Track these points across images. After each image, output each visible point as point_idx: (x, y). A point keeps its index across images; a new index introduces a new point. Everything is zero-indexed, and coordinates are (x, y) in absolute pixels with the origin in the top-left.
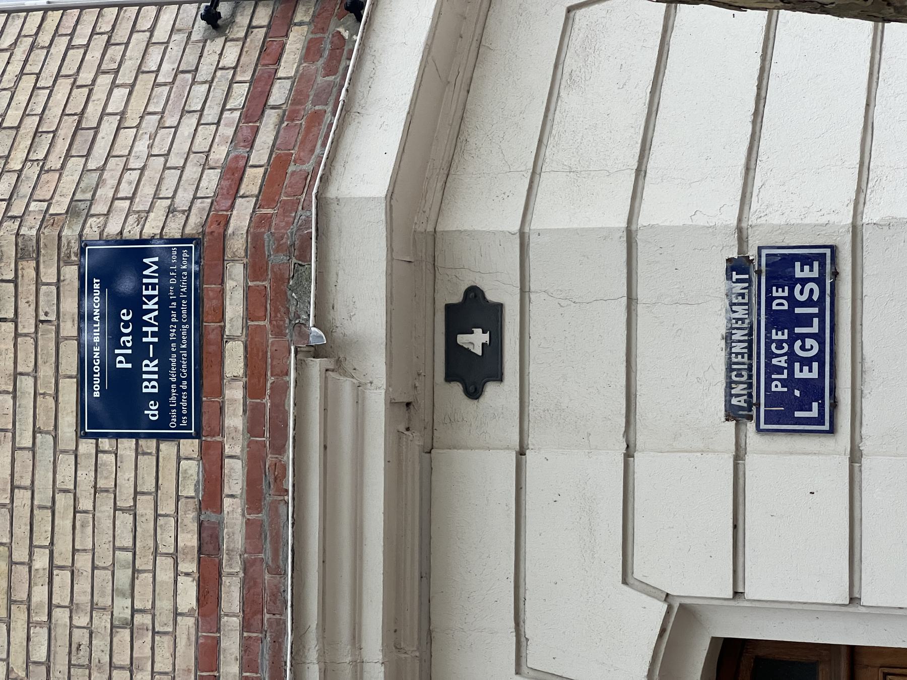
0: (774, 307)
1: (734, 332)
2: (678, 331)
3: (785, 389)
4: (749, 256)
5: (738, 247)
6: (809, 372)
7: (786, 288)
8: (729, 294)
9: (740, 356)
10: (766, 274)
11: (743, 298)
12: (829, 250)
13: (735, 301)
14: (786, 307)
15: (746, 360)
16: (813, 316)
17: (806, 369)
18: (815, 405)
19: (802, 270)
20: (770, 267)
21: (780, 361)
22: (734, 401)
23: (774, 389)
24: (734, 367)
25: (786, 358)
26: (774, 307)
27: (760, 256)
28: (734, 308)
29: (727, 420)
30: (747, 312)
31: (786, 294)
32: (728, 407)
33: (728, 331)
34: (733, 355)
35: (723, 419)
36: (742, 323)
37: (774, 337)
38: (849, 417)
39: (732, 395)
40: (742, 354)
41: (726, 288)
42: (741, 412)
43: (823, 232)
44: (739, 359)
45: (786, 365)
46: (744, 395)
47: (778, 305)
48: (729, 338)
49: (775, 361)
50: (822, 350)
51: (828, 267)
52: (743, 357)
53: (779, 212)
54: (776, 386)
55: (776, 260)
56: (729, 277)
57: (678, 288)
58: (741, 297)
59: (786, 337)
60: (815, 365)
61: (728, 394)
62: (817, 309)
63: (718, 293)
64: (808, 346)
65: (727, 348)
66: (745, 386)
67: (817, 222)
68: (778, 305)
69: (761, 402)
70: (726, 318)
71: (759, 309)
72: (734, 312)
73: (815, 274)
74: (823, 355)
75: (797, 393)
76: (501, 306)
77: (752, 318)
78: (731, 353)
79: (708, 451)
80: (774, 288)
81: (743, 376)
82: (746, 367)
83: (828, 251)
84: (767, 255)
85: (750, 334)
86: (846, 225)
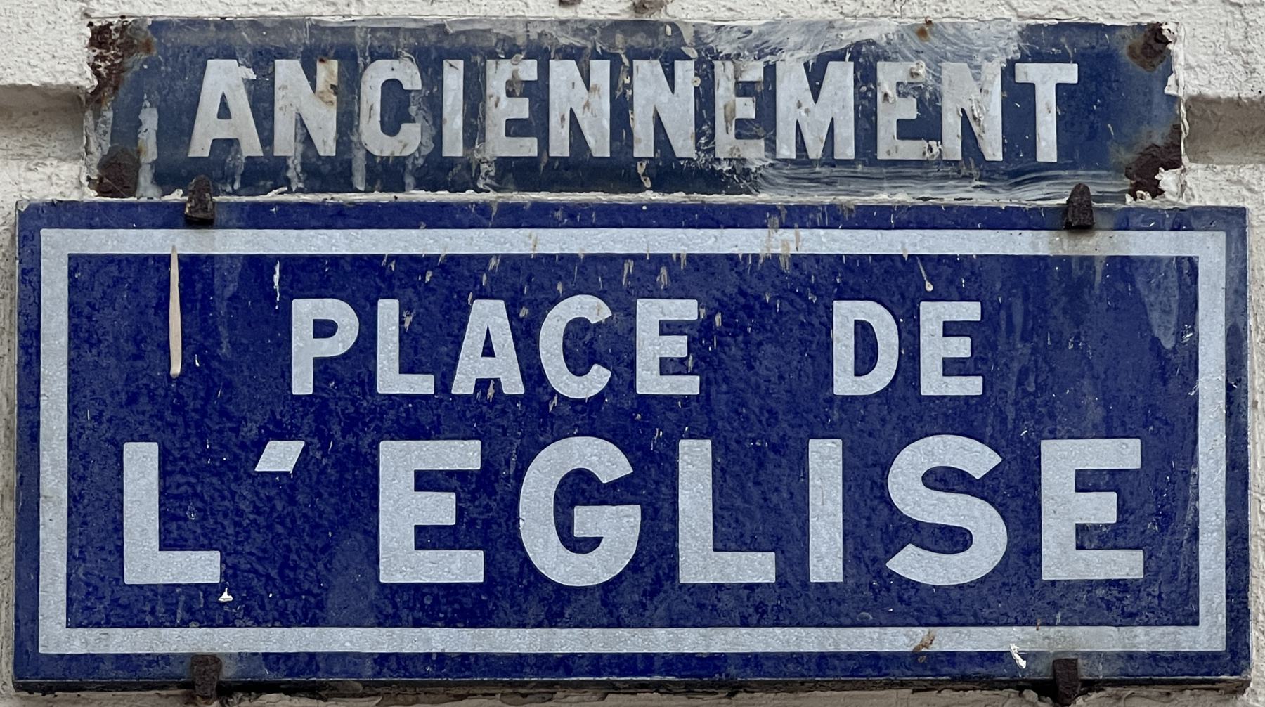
0: (846, 313)
1: (685, 71)
3: (303, 384)
4: (1174, 164)
6: (419, 530)
7: (972, 386)
8: (935, 41)
9: (521, 108)
10: (1065, 261)
11: (906, 130)
12: (1219, 645)
13: (889, 76)
14: (846, 383)
15: (499, 145)
19: (1086, 482)
20: (1107, 285)
21: (488, 351)
23: (305, 311)
24: (454, 77)
25: (514, 385)
26: (846, 313)
27: (1183, 220)
28: (841, 76)
29: (100, 37)
30: (815, 151)
31: (933, 383)
32: (189, 38)
33: (688, 36)
34: (529, 70)
36: (741, 123)
37: (650, 312)
39: (263, 60)
40: (536, 125)
42: (150, 119)
45: (463, 385)
46: (267, 139)
48: (640, 40)
52: (515, 128)
54: (324, 329)
55: (1155, 317)
58: (912, 114)
59: (649, 382)
61: (274, 41)
64: (586, 519)
65: (576, 32)
66: (327, 146)
68: (864, 332)
69: (219, 234)
70: (774, 24)
71: (834, 218)
72: (816, 74)
74: (534, 609)
76: (1032, 86)
78: (542, 54)
80: (970, 311)
81: (391, 127)
82: (454, 147)
84: (1188, 269)
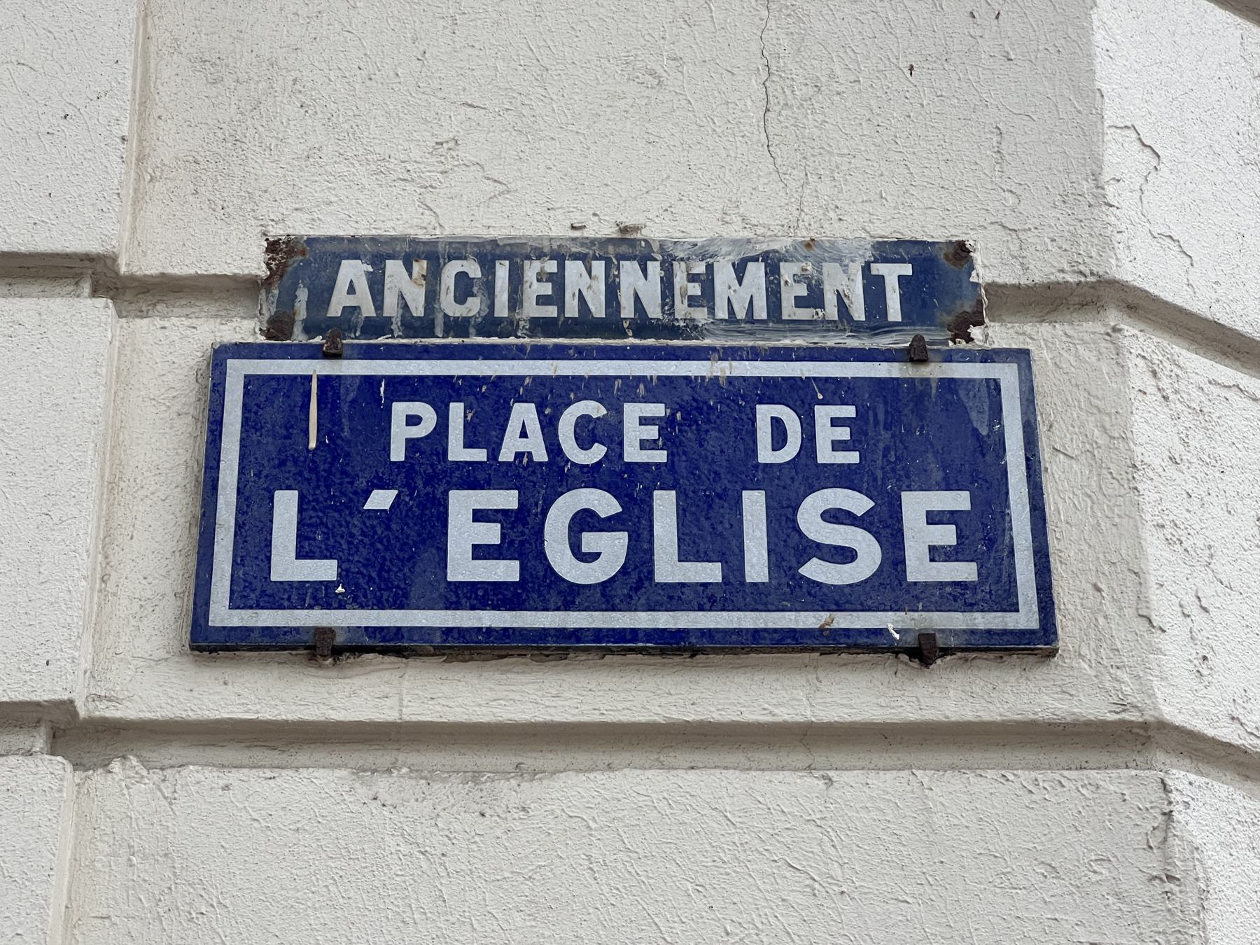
0: (765, 413)
1: (654, 268)
2: (653, 74)
4: (980, 323)
5: (1018, 287)
7: (853, 457)
8: (817, 251)
9: (547, 289)
10: (911, 381)
13: (787, 271)
14: (766, 455)
15: (531, 309)
16: (732, 557)
17: (491, 534)
18: (326, 570)
20: (939, 396)
21: (524, 434)
22: (353, 271)
23: (400, 410)
24: (502, 271)
25: (541, 455)
26: (765, 413)
27: (988, 356)
28: (756, 272)
29: (273, 247)
30: (741, 314)
31: (825, 455)
32: (329, 247)
33: (656, 247)
34: (552, 267)
35: (277, 232)
36: (691, 298)
37: (632, 412)
38: (267, 714)
39: (378, 261)
40: (557, 298)
41: (840, 241)
42: (303, 295)
43: (1109, 608)
44: (535, 288)
45: (506, 455)
46: (379, 304)
47: (777, 423)
48: (624, 249)
49: (524, 413)
50: (571, 596)
51: (957, 620)
52: (542, 300)
53: (1179, 449)
54: (413, 420)
55: (974, 415)
56: (888, 251)
57: (832, 76)
59: (632, 454)
60: (507, 571)
62: (764, 578)
63: (819, 213)
64: (590, 541)
66: (418, 309)
67: (1152, 580)
68: (777, 423)
70: (712, 241)
71: (755, 354)
72: (740, 270)
73: (919, 569)
74: (554, 598)
75: (381, 500)
77: (712, 334)
79: (139, 178)
81: (460, 299)
82: (502, 311)
83: (1026, 618)
84: (994, 387)
85: (643, 326)
86: (1152, 696)
